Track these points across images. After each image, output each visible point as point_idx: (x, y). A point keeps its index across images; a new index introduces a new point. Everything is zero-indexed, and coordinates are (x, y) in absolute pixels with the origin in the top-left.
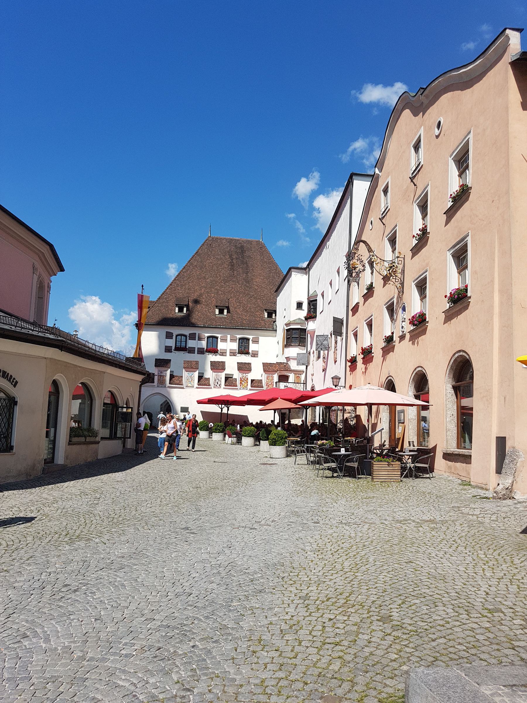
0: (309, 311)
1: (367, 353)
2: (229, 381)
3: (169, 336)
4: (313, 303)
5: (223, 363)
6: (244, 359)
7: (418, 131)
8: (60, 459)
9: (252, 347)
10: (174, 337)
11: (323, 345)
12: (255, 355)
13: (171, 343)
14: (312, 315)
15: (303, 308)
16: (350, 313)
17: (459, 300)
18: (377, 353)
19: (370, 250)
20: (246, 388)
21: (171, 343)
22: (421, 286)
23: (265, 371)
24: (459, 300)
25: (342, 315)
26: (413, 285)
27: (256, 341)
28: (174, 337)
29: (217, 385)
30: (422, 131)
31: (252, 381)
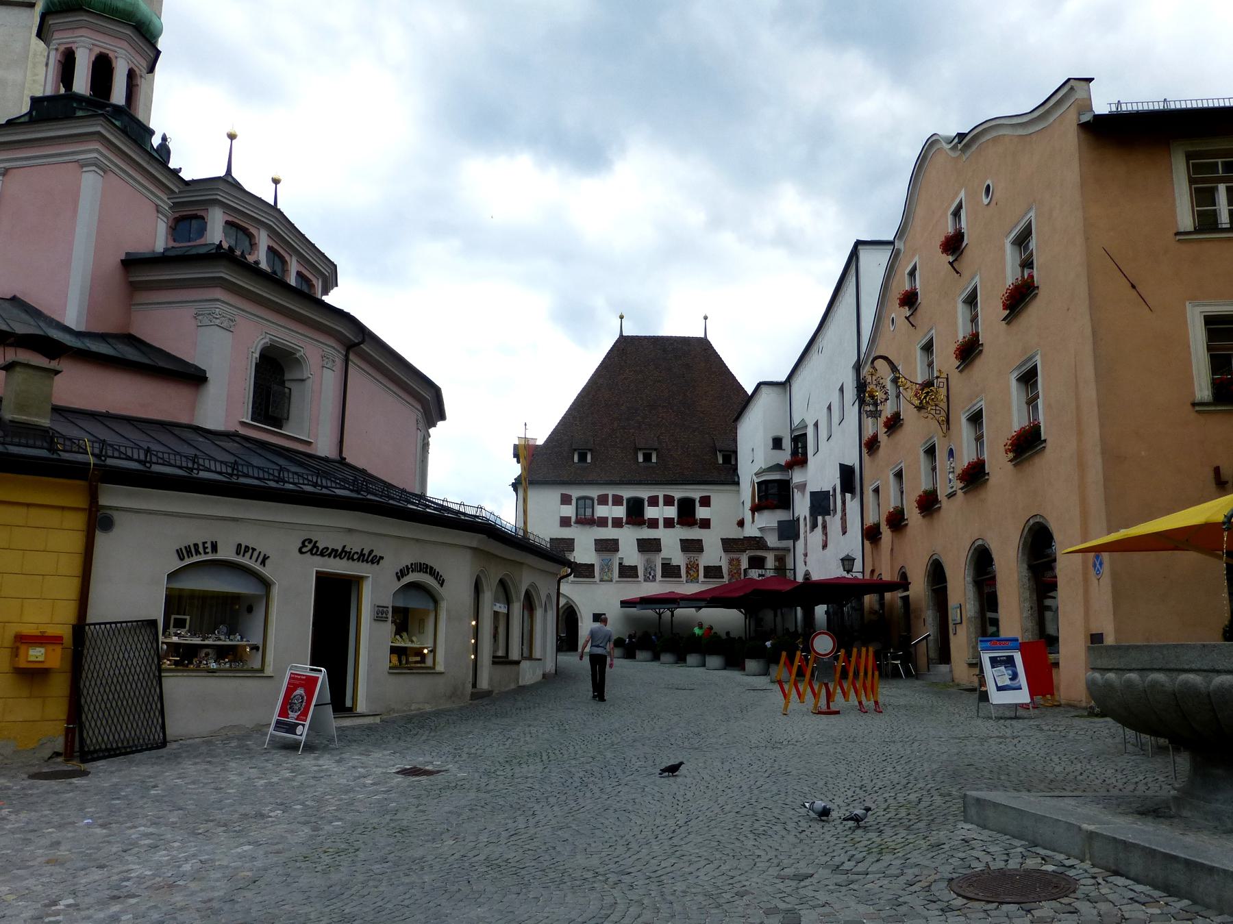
0: (794, 453)
1: (897, 521)
2: (670, 571)
3: (566, 500)
4: (799, 440)
5: (658, 541)
6: (693, 533)
7: (957, 194)
8: (484, 684)
9: (702, 513)
10: (574, 502)
11: (821, 504)
12: (705, 524)
13: (569, 511)
14: (799, 459)
15: (784, 446)
16: (865, 450)
17: (1027, 444)
18: (913, 515)
19: (894, 369)
20: (696, 580)
21: (569, 511)
22: (976, 419)
23: (725, 550)
24: (1027, 444)
25: (852, 459)
26: (964, 420)
27: (706, 502)
28: (574, 502)
29: (650, 578)
30: (962, 194)
31: (707, 568)
